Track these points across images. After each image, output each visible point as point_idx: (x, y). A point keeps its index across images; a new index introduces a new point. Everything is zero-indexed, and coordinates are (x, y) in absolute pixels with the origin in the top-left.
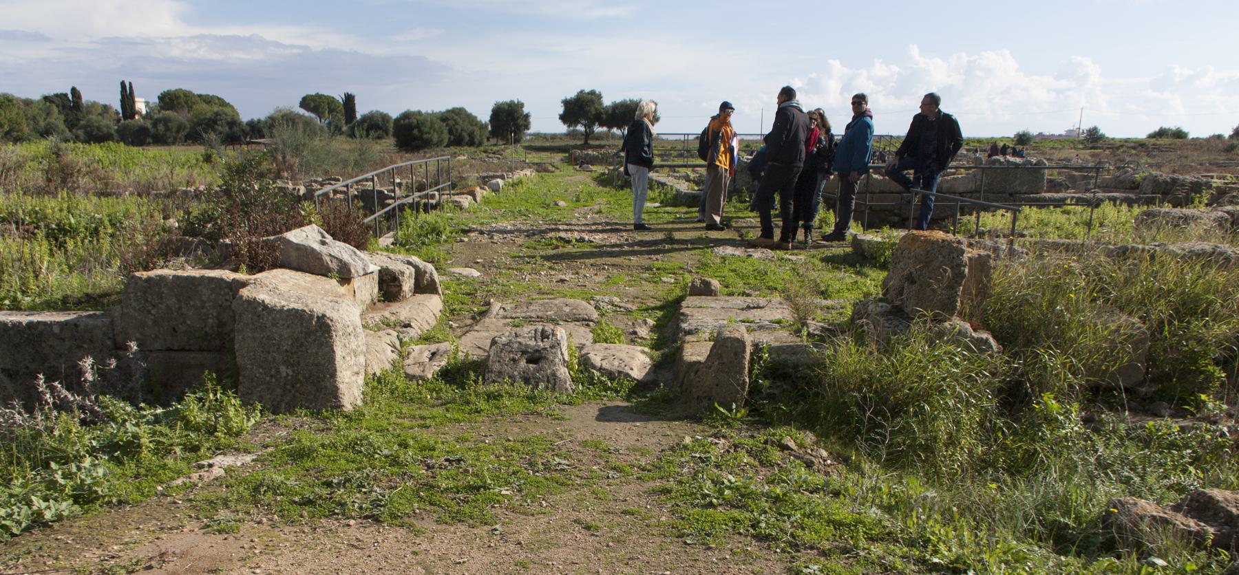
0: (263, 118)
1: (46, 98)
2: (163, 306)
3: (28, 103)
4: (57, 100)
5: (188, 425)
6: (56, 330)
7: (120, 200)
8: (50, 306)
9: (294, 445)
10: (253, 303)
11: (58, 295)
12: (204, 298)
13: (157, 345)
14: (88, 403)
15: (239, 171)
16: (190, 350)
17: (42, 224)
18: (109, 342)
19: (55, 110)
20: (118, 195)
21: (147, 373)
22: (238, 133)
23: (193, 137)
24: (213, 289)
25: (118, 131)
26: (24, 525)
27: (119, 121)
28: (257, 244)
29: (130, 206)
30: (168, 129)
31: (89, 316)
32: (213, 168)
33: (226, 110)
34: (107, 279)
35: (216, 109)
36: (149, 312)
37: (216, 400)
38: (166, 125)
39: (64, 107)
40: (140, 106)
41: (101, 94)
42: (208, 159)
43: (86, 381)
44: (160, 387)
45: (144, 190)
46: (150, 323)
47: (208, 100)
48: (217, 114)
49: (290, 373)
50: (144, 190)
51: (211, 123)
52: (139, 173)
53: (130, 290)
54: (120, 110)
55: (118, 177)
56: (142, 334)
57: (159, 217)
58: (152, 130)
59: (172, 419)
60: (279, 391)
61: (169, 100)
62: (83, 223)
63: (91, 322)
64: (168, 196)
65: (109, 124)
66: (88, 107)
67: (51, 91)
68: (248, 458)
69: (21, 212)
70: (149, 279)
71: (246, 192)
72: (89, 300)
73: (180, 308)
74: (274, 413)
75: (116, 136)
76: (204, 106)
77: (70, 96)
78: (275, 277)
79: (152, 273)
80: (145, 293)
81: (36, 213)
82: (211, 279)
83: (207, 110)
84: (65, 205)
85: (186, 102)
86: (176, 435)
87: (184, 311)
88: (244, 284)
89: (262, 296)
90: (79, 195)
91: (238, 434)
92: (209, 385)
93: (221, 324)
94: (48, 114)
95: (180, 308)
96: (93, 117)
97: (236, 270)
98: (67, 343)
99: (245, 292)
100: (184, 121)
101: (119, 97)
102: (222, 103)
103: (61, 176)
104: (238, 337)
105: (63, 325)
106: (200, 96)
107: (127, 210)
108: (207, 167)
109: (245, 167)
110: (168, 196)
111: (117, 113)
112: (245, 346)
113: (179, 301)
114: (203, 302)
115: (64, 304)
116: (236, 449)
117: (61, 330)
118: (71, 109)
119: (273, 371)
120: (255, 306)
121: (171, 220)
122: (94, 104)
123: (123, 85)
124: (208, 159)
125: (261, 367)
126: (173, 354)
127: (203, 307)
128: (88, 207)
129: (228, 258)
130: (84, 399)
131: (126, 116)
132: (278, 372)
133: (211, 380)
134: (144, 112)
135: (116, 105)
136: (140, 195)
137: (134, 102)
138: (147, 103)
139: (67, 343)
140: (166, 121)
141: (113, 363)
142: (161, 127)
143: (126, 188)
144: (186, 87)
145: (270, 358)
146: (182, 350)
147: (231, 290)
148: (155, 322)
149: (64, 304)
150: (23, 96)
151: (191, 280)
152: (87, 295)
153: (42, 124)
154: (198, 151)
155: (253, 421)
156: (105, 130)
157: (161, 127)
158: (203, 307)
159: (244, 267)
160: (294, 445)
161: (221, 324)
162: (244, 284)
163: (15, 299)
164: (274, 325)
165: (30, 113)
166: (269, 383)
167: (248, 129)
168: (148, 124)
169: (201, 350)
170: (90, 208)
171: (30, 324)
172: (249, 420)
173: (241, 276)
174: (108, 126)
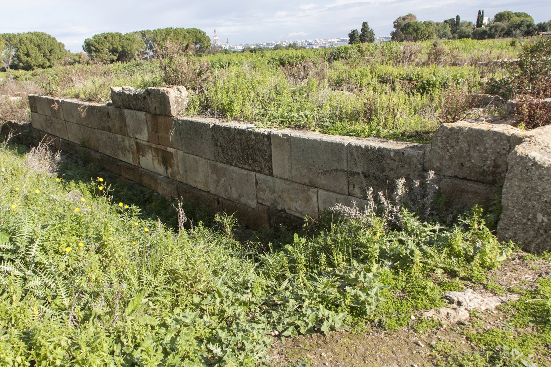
0: (546, 22)
1: (445, 21)
2: (458, 148)
3: (438, 24)
4: (450, 22)
5: (453, 253)
6: (392, 154)
7: (461, 68)
8: (395, 137)
9: (538, 299)
10: (524, 159)
11: (401, 130)
12: (487, 146)
13: (449, 173)
14: (395, 210)
15: (533, 51)
16: (470, 180)
17: (420, 80)
18: (420, 166)
19: (448, 26)
20: (460, 65)
21: (439, 193)
22: (530, 30)
23: (508, 33)
24: (495, 140)
25: (473, 34)
26: (310, 325)
27: (474, 29)
28: (537, 105)
29: (466, 70)
30: (496, 31)
31: (413, 148)
32: (515, 48)
33: (527, 19)
34: (430, 122)
35: (522, 19)
36: (448, 150)
37: (479, 229)
38: (495, 29)
39: (452, 25)
40: (485, 21)
41: (469, 18)
42: (513, 44)
43: (397, 194)
44: (443, 209)
45: (474, 62)
46: (447, 158)
47: (518, 15)
48: (522, 21)
49: (546, 220)
50: (474, 62)
51: (519, 26)
52: (475, 53)
53: (439, 135)
54: (476, 24)
55: (464, 55)
56: (441, 164)
57: (478, 76)
58: (489, 32)
59: (441, 243)
60: (532, 233)
61: (500, 17)
62: (439, 80)
63: (411, 152)
64: (486, 65)
65: (470, 31)
66: (462, 23)
67: (447, 18)
68: (492, 302)
69: (412, 75)
70: (452, 129)
71: (533, 64)
72: (417, 136)
73: (469, 151)
74: (524, 250)
75: (472, 36)
76: (517, 18)
77: (455, 20)
78: (546, 133)
79: (455, 125)
80: (448, 137)
81: (419, 75)
82: (495, 133)
83: (517, 20)
84: (433, 71)
85: (508, 17)
86: (439, 259)
87: (471, 153)
88: (520, 140)
89: (535, 154)
90: (440, 66)
91: (489, 268)
92: (476, 218)
93: (496, 166)
94: (445, 28)
95: (469, 151)
96: (463, 28)
97: (515, 125)
98: (397, 163)
99: (520, 149)
100: (505, 26)
101: (477, 18)
102: (526, 15)
103: (435, 56)
104: (507, 184)
105: (397, 152)
106: (515, 13)
107: (463, 73)
108: (511, 48)
109: (538, 47)
110: (486, 65)
111: (474, 25)
112: (511, 191)
113: (469, 146)
114: (486, 149)
115: (402, 137)
116: (485, 287)
117: (395, 155)
118: (455, 25)
119: (530, 216)
120: (529, 165)
121: (484, 78)
122: (465, 22)
123: (479, 12)
124: (513, 44)
125: (520, 210)
126: (458, 181)
127: (485, 152)
128: (444, 72)
129: (512, 115)
130: (393, 207)
131: (477, 27)
132: (535, 217)
133: (478, 212)
134: (486, 24)
135: (475, 22)
136: (471, 65)
137: (483, 19)
138: (489, 19)
139: (397, 163)
140: (496, 27)
141: (417, 183)
142: (493, 30)
143: (465, 61)
144: (509, 10)
145: (530, 205)
146: (465, 179)
147: (509, 141)
148: (451, 157)
149: (402, 137)
150: (436, 22)
151: (480, 133)
152: (416, 132)
153: (442, 32)
154: (508, 40)
155: (504, 257)
156: (467, 33)
157: (493, 30)
158: (485, 152)
159: (523, 124)
160: (538, 299)
161: (496, 166)
162: (520, 140)
163: (378, 131)
164: (540, 179)
165: (438, 28)
166: (525, 224)
167: (537, 27)
168: (487, 29)
169: (477, 181)
170: (444, 72)
171: (380, 150)
172: (501, 254)
173: (520, 131)
174: (469, 32)
